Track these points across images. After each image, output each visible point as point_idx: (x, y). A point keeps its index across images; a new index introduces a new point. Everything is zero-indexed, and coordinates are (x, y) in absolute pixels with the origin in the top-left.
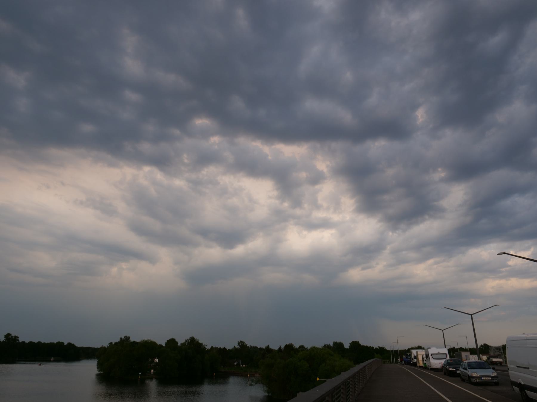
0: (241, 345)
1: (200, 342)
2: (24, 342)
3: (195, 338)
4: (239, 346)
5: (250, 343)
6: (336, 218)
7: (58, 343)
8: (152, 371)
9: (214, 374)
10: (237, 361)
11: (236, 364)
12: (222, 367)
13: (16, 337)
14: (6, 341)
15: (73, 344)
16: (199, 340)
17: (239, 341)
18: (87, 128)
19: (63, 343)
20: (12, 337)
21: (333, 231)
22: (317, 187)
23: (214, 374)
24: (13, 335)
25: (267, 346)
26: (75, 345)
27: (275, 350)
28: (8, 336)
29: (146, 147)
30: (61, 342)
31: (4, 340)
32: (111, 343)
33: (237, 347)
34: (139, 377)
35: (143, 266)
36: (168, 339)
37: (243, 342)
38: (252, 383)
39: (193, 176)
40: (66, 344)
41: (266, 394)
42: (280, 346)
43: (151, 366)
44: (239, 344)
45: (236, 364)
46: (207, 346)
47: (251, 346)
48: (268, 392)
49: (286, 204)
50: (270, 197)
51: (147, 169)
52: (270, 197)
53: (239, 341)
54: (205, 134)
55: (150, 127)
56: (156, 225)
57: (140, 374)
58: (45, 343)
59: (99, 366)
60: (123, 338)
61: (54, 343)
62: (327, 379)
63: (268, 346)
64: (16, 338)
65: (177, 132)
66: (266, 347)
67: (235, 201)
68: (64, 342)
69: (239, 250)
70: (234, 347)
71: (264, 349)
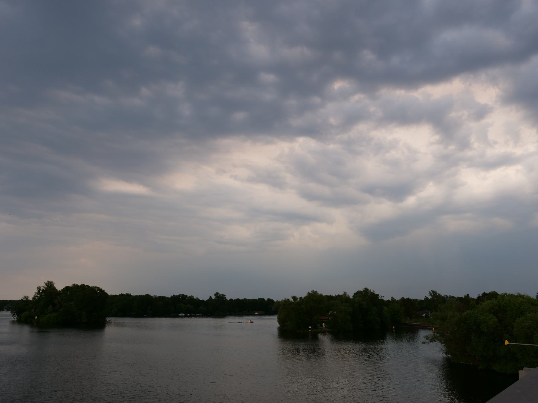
0: (433, 295)
1: (376, 293)
2: (231, 300)
3: (369, 288)
4: (431, 296)
5: (443, 293)
6: (518, 151)
7: (260, 299)
8: (324, 324)
9: (394, 327)
10: (426, 312)
11: (424, 315)
12: (409, 319)
13: (223, 295)
14: (216, 299)
15: (272, 300)
16: (375, 291)
17: (431, 291)
18: (240, 116)
19: (264, 299)
20: (220, 295)
21: (519, 167)
22: (484, 121)
23: (394, 327)
24: (220, 294)
25: (466, 295)
26: (240, 299)
27: (473, 299)
28: (217, 294)
29: (296, 122)
30: (262, 299)
31: (215, 298)
32: (286, 299)
33: (430, 297)
34: (310, 331)
35: (322, 227)
36: (355, 292)
37: (435, 291)
38: (426, 341)
39: (345, 136)
40: (266, 300)
41: (445, 355)
42: (45, 283)
43: (330, 319)
44: (430, 294)
45: (424, 315)
46: (384, 297)
47: (447, 296)
48: (446, 353)
49: (452, 147)
50: (432, 144)
51: (301, 140)
52: (432, 144)
53: (431, 291)
54: (344, 95)
55: (292, 102)
56: (325, 191)
57: (310, 327)
58: (249, 299)
59: (280, 321)
60: (310, 292)
61: (256, 299)
62: (508, 344)
63: (468, 295)
64: (223, 297)
65: (317, 100)
66: (465, 296)
67: (394, 154)
68: (264, 298)
69: (411, 201)
70: (425, 297)
71: (333, 297)
